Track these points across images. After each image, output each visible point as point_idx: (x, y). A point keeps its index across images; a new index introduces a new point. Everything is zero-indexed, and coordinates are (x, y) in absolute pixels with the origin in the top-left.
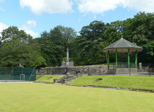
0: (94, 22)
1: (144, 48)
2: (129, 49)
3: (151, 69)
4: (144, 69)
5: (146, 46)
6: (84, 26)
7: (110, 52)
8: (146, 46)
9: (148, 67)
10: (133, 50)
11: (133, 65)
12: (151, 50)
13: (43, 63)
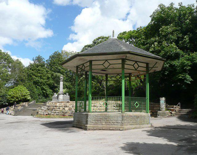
0: (99, 38)
1: (171, 66)
2: (124, 61)
3: (185, 111)
4: (171, 110)
5: (176, 63)
6: (86, 44)
7: (78, 72)
8: (176, 63)
9: (179, 105)
10: (136, 62)
11: (137, 105)
12: (185, 71)
13: (25, 96)
